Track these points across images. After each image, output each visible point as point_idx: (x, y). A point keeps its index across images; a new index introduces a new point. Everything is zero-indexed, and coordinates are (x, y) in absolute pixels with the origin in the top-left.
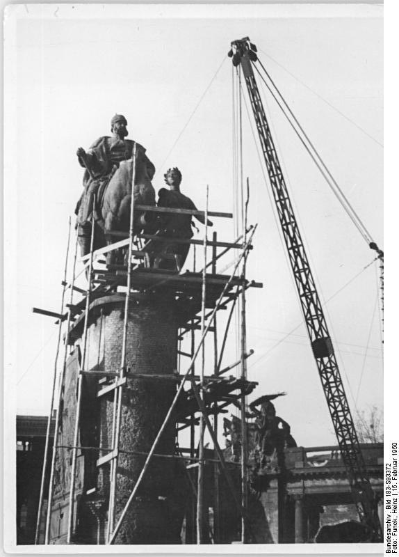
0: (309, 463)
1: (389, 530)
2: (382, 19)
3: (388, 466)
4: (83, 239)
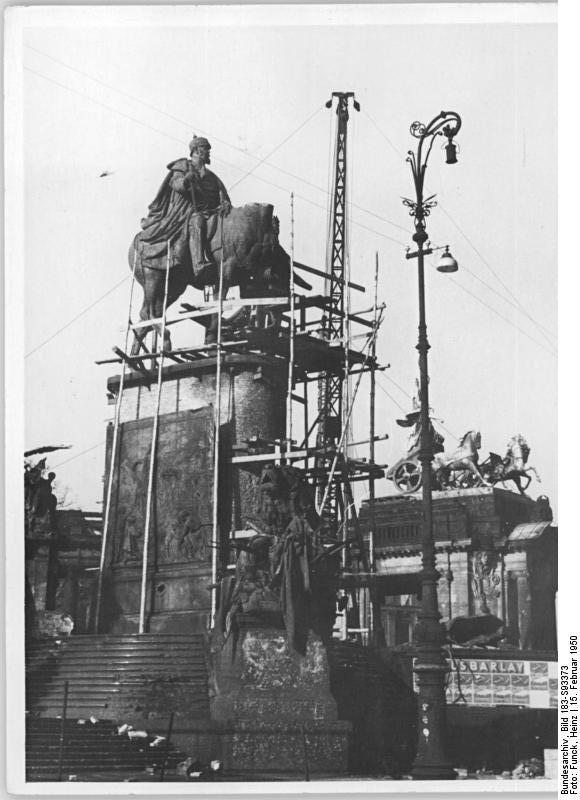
0: (89, 530)
1: (566, 761)
2: (555, 25)
3: (564, 670)
4: (203, 376)
